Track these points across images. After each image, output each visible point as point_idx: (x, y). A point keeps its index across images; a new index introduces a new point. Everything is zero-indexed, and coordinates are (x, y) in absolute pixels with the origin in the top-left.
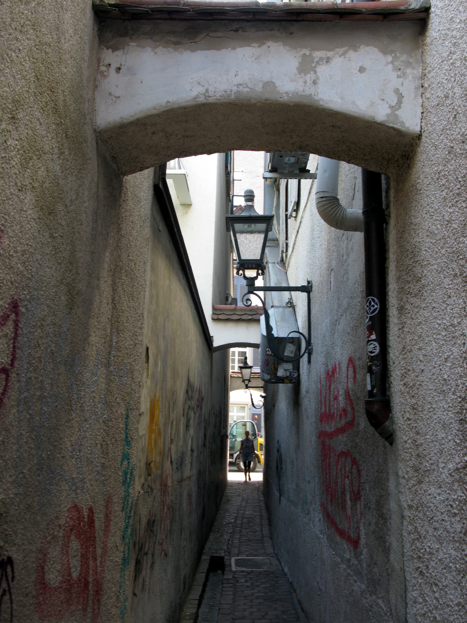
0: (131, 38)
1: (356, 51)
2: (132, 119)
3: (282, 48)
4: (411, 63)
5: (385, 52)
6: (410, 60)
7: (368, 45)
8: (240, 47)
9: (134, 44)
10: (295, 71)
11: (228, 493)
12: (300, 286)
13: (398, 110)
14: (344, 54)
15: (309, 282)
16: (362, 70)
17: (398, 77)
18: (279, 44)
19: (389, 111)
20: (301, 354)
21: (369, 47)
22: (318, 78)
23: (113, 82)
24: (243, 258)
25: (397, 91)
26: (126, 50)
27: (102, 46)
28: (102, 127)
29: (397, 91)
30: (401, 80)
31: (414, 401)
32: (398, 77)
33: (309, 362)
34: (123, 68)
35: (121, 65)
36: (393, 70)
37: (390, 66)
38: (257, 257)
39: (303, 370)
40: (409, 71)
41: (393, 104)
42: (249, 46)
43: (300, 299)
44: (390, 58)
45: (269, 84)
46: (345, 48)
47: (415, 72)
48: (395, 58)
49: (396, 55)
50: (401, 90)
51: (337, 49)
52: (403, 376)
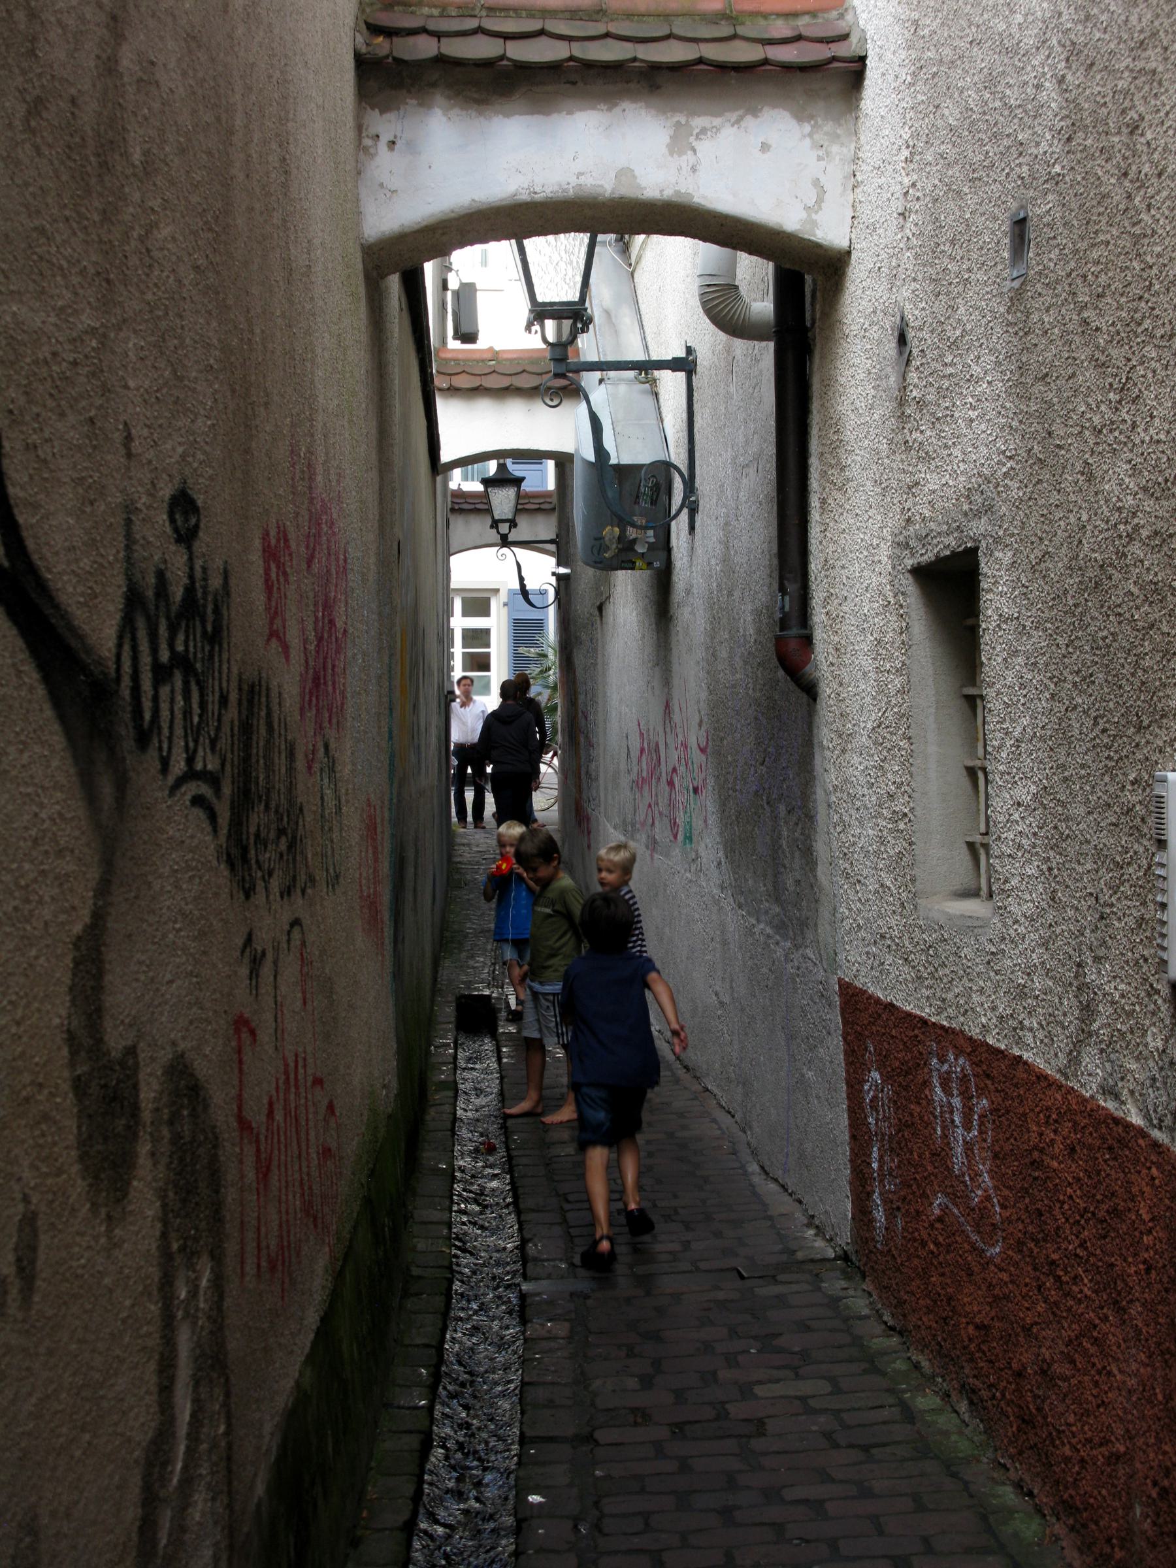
0: (409, 91)
1: (756, 116)
2: (417, 227)
3: (643, 112)
4: (838, 136)
5: (800, 118)
6: (839, 131)
7: (774, 107)
8: (581, 110)
9: (414, 102)
10: (664, 150)
11: (460, 863)
12: (669, 358)
13: (816, 212)
14: (738, 122)
15: (689, 350)
16: (765, 148)
17: (819, 159)
18: (639, 105)
19: (804, 215)
20: (673, 512)
21: (776, 110)
22: (698, 162)
23: (385, 165)
24: (540, 299)
25: (816, 182)
26: (402, 112)
27: (364, 104)
28: (371, 240)
29: (816, 182)
30: (823, 163)
31: (836, 639)
32: (819, 159)
33: (692, 528)
34: (399, 142)
35: (395, 137)
36: (812, 148)
37: (808, 141)
38: (573, 295)
39: (678, 538)
40: (835, 149)
41: (811, 203)
42: (594, 108)
43: (671, 384)
44: (807, 128)
45: (625, 173)
46: (740, 112)
47: (845, 150)
48: (815, 127)
49: (816, 123)
50: (823, 180)
51: (727, 114)
52: (826, 601)
